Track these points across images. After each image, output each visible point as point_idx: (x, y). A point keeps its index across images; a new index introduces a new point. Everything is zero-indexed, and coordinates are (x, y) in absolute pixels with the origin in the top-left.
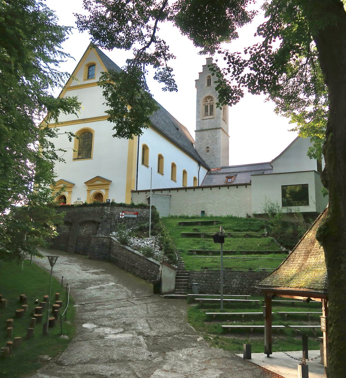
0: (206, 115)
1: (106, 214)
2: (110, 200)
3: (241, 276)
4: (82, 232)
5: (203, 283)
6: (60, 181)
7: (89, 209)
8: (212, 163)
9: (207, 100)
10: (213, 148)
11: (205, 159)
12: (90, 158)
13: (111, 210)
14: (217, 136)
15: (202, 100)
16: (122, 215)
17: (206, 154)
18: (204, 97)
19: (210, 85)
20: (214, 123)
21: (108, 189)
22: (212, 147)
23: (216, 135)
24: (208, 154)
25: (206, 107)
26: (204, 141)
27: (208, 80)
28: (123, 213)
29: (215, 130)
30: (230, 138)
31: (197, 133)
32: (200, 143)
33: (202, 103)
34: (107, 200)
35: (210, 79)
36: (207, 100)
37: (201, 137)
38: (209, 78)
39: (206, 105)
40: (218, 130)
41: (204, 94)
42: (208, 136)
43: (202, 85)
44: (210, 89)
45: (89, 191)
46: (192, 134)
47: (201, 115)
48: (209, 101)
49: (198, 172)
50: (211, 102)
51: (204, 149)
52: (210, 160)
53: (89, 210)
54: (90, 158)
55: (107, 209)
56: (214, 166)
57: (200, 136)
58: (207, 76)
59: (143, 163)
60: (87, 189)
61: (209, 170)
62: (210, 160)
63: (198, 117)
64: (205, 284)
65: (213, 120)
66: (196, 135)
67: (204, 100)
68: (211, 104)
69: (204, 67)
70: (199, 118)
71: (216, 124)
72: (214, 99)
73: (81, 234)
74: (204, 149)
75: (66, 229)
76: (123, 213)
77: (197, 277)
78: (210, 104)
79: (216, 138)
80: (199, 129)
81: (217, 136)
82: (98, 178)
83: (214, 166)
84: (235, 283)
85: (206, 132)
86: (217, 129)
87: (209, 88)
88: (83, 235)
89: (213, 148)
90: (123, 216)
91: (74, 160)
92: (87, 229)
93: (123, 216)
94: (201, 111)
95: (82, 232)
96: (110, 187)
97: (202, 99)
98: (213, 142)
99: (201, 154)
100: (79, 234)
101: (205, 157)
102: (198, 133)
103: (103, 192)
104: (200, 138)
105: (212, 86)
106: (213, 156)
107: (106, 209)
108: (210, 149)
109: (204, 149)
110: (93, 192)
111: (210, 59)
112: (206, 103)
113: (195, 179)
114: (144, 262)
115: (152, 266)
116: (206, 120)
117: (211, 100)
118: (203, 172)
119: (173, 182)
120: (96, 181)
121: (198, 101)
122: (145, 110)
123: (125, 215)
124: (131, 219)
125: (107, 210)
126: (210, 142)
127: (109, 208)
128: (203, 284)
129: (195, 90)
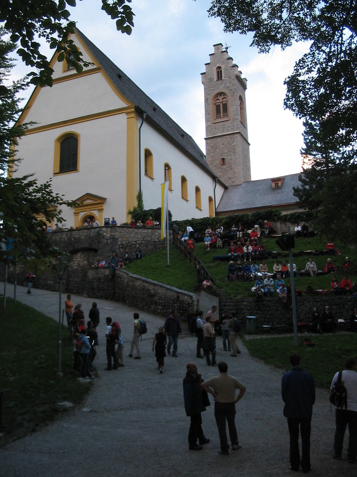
1: (106, 238)
2: (109, 219)
3: (311, 301)
5: (258, 314)
7: (82, 232)
8: (230, 179)
12: (76, 170)
13: (111, 232)
17: (221, 168)
18: (214, 94)
19: (221, 78)
21: (102, 210)
23: (233, 143)
25: (218, 107)
26: (217, 150)
27: (218, 72)
30: (250, 146)
31: (207, 141)
32: (212, 154)
33: (210, 101)
34: (105, 219)
35: (221, 71)
36: (218, 98)
37: (213, 146)
39: (217, 104)
42: (223, 144)
45: (76, 214)
46: (202, 146)
49: (213, 191)
50: (224, 100)
51: (218, 161)
52: (228, 176)
53: (81, 233)
54: (76, 170)
56: (233, 183)
57: (212, 145)
60: (74, 211)
61: (226, 188)
62: (228, 176)
63: (207, 120)
64: (261, 316)
66: (207, 144)
68: (224, 103)
69: (212, 56)
70: (209, 121)
71: (232, 128)
72: (228, 97)
74: (218, 162)
82: (89, 196)
84: (304, 312)
85: (219, 139)
87: (220, 82)
88: (76, 267)
89: (231, 159)
91: (56, 175)
92: (80, 259)
96: (105, 207)
102: (209, 141)
103: (95, 213)
104: (212, 148)
105: (224, 80)
106: (231, 169)
108: (226, 161)
110: (82, 215)
111: (219, 46)
112: (218, 101)
113: (210, 199)
114: (167, 294)
116: (219, 123)
118: (220, 191)
120: (85, 200)
122: (111, 260)
125: (106, 232)
126: (226, 151)
127: (109, 229)
128: (259, 315)
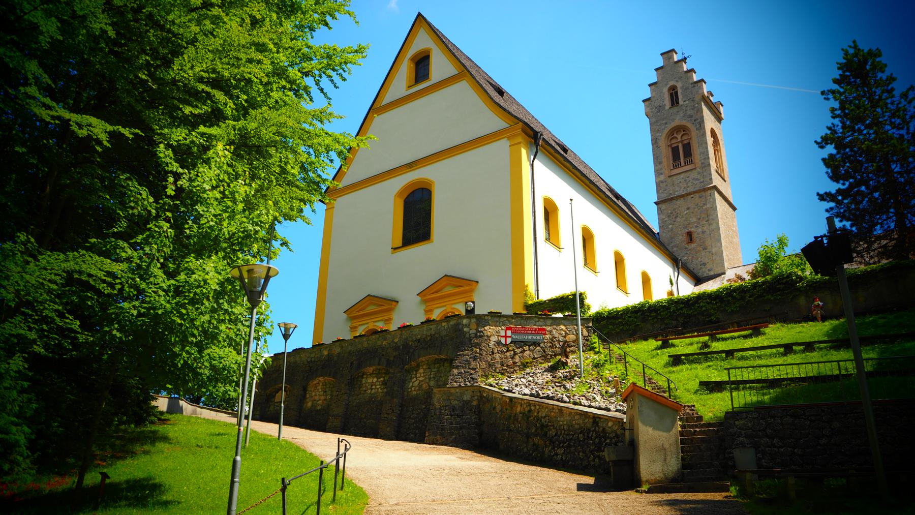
0: (675, 167)
4: (412, 386)
6: (368, 297)
8: (704, 264)
9: (675, 135)
10: (703, 232)
11: (686, 258)
14: (708, 206)
15: (663, 137)
16: (506, 337)
18: (666, 131)
19: (678, 103)
20: (697, 179)
22: (700, 230)
24: (693, 245)
25: (675, 151)
26: (678, 219)
27: (671, 95)
28: (508, 331)
29: (703, 194)
32: (670, 226)
33: (663, 143)
36: (675, 135)
37: (671, 213)
38: (674, 90)
40: (709, 192)
41: (666, 123)
42: (688, 209)
43: (660, 106)
44: (678, 112)
47: (666, 167)
48: (679, 137)
50: (685, 138)
55: (469, 325)
56: (709, 270)
57: (669, 212)
58: (668, 86)
59: (548, 239)
63: (658, 173)
65: (694, 174)
67: (669, 137)
68: (685, 142)
70: (662, 174)
71: (702, 180)
73: (411, 391)
74: (681, 238)
75: (376, 386)
76: (508, 331)
77: (751, 429)
78: (682, 141)
79: (707, 210)
80: (664, 196)
81: (708, 206)
83: (709, 270)
85: (680, 202)
86: (705, 190)
87: (675, 109)
90: (507, 335)
93: (507, 335)
94: (664, 160)
95: (412, 386)
97: (664, 136)
98: (700, 219)
99: (675, 249)
100: (406, 393)
101: (687, 253)
107: (466, 325)
108: (695, 236)
109: (680, 237)
112: (674, 141)
115: (597, 428)
117: (682, 133)
119: (620, 294)
121: (655, 142)
123: (514, 337)
124: (529, 346)
126: (694, 220)
129: (647, 121)
